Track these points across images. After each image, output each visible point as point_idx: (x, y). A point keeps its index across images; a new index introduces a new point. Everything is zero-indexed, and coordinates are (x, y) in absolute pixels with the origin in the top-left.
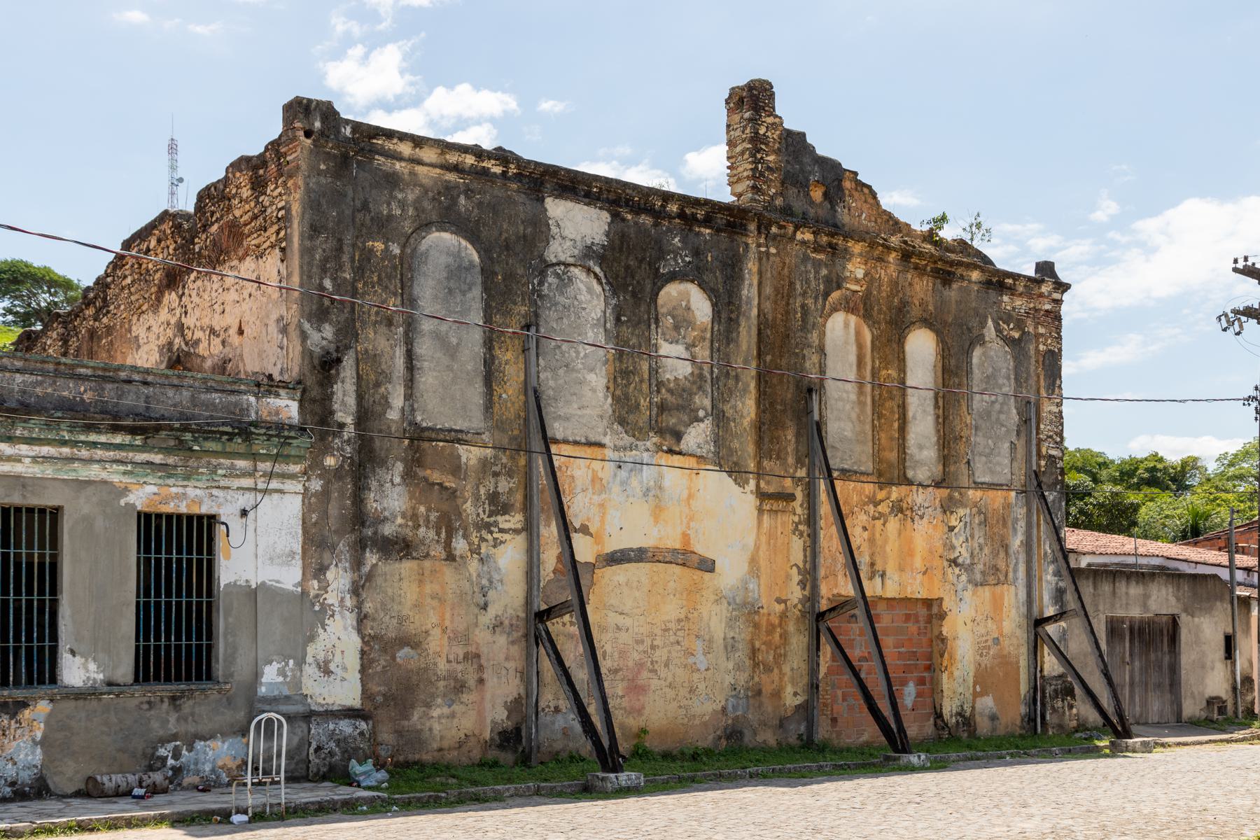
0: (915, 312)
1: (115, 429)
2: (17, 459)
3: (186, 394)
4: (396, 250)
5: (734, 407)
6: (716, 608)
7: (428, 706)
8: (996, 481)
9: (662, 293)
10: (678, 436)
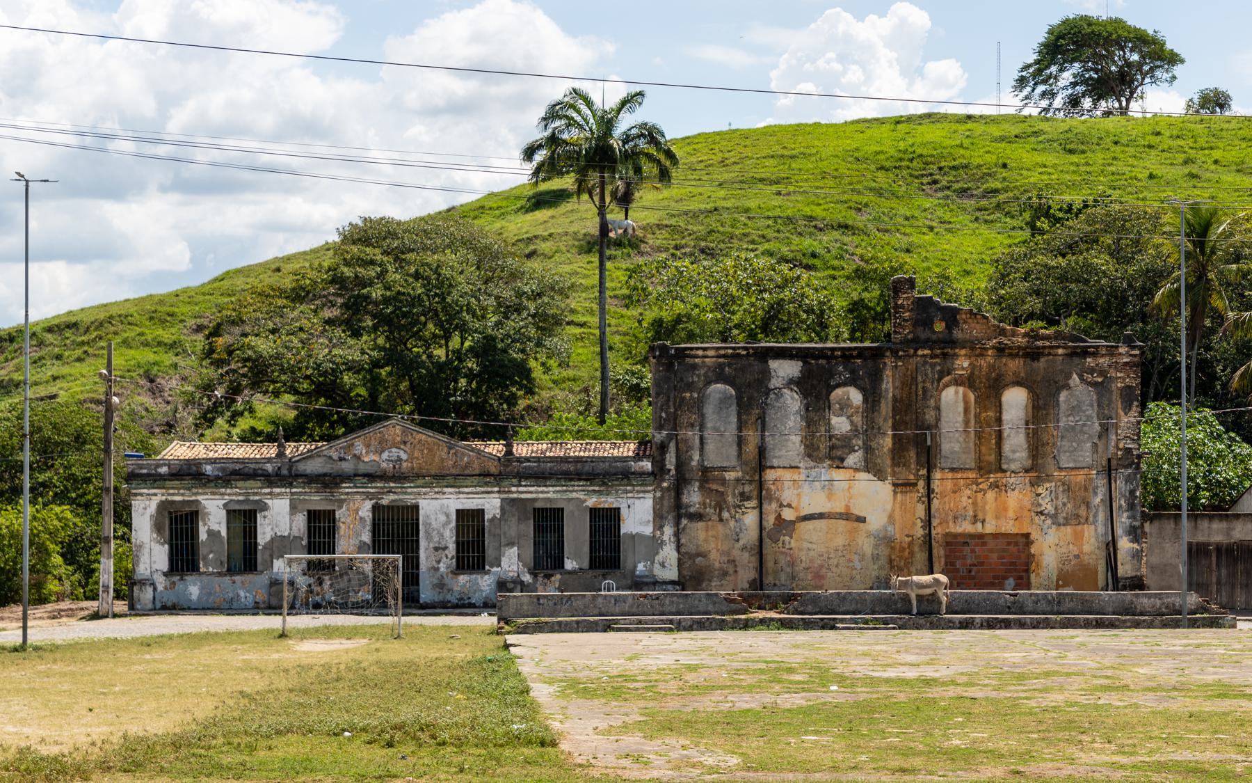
0: (1010, 378)
1: (580, 480)
2: (548, 492)
3: (607, 464)
4: (695, 395)
5: (878, 444)
6: (866, 540)
7: (710, 581)
8: (1078, 465)
9: (833, 394)
10: (842, 460)
